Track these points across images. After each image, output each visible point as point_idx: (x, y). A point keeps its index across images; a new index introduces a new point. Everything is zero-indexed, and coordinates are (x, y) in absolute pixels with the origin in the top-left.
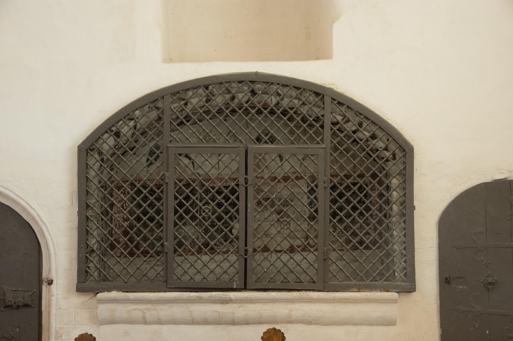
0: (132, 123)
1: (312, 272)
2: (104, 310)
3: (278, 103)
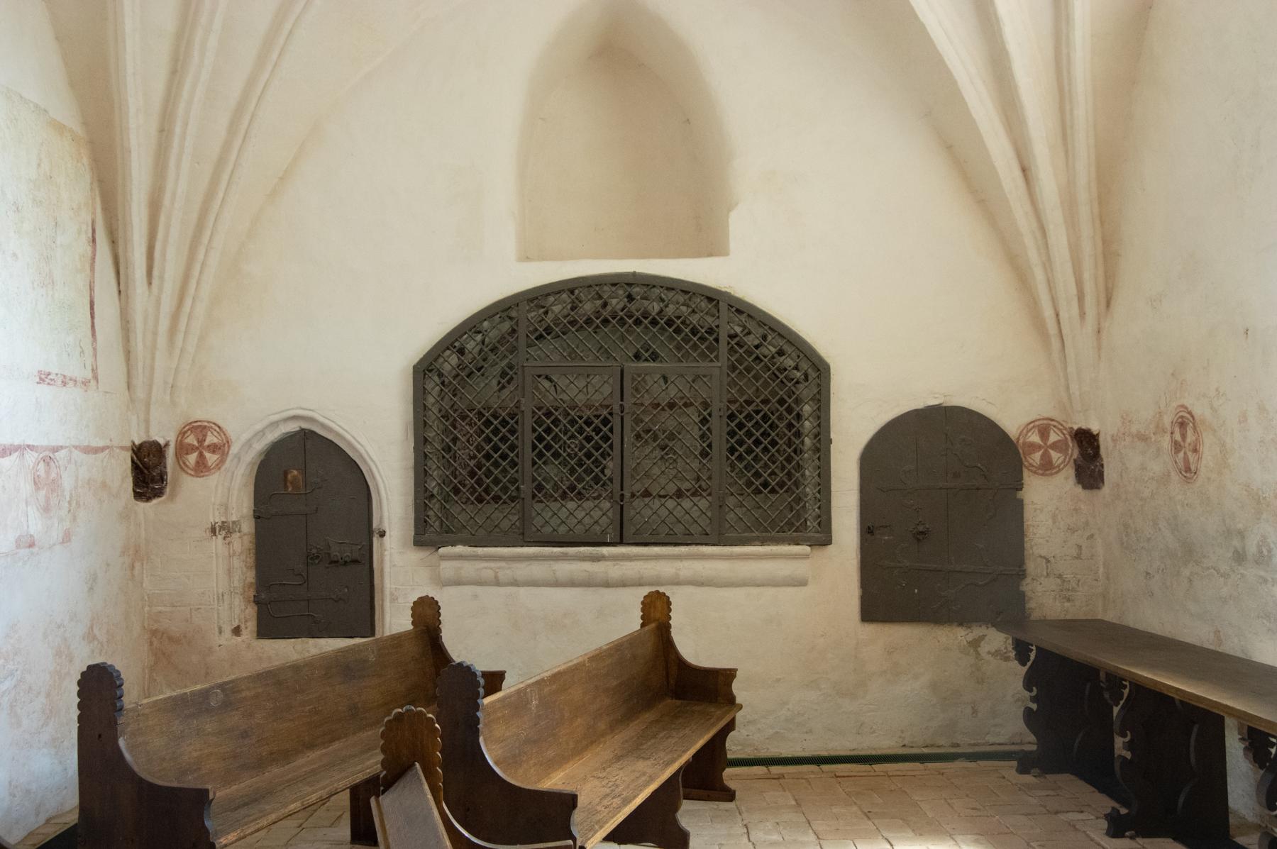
0: (479, 337)
1: (704, 522)
2: (448, 568)
3: (661, 311)
